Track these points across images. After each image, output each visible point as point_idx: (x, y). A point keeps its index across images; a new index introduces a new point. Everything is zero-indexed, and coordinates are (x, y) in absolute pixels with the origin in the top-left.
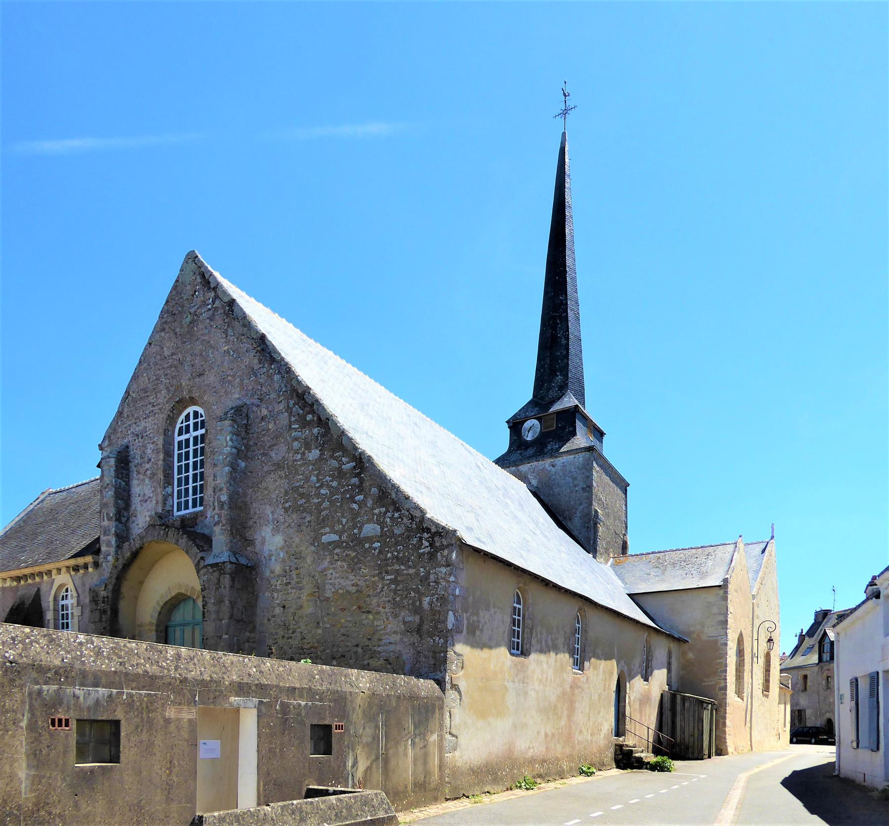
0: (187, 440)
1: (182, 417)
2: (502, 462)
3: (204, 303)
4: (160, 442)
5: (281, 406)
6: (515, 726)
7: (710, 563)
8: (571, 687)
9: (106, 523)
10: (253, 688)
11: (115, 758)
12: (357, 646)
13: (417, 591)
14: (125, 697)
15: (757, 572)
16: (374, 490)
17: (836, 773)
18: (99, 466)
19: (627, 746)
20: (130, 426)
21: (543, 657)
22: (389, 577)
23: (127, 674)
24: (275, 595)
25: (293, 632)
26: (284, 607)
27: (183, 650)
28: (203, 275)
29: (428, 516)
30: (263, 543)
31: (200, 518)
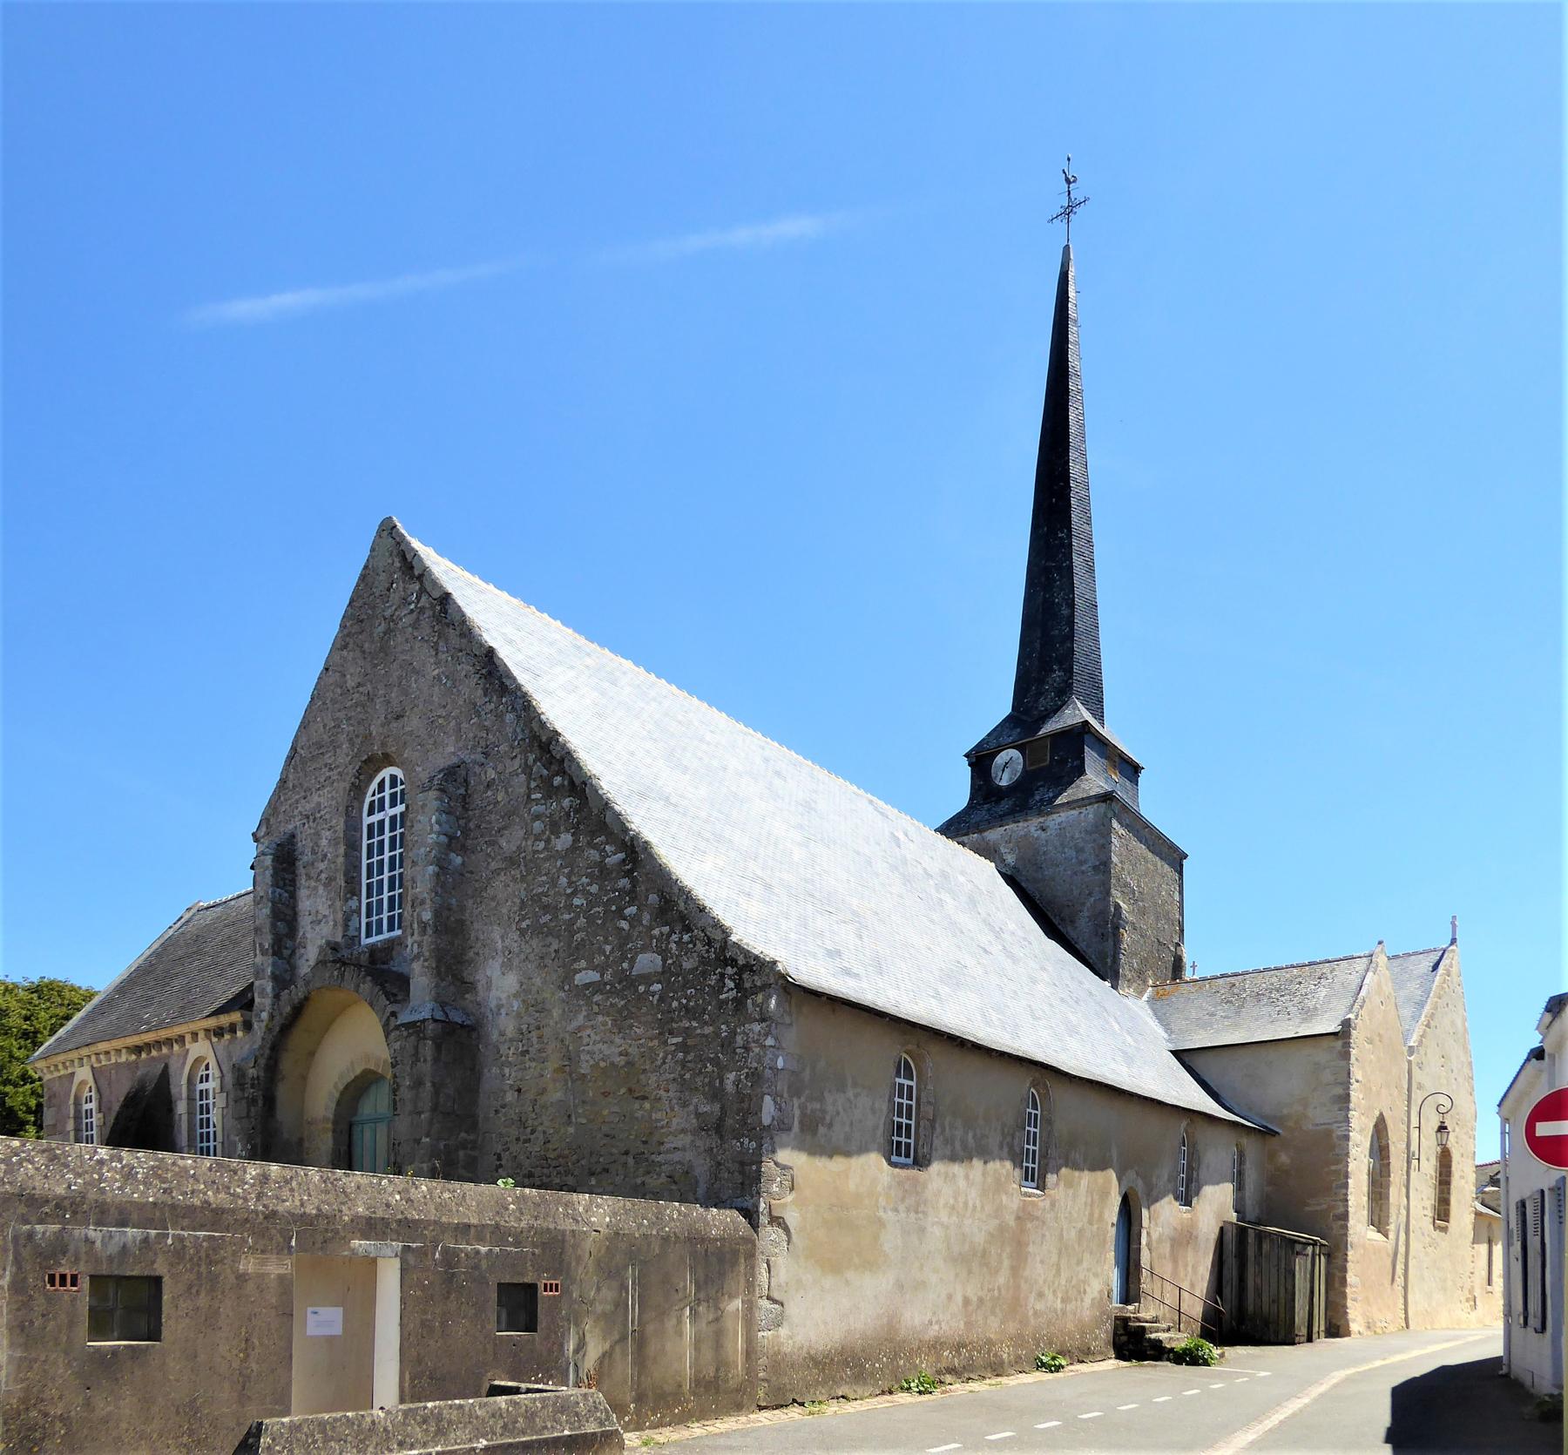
0: (381, 823)
1: (374, 785)
2: (953, 829)
3: (405, 601)
4: (341, 827)
5: (517, 763)
6: (900, 1286)
7: (1323, 992)
8: (1018, 1218)
9: (259, 959)
10: (394, 1225)
11: (154, 1335)
12: (627, 1153)
13: (716, 1062)
14: (170, 1241)
15: (1421, 1005)
16: (653, 898)
17: (1504, 1370)
18: (252, 867)
19: (1138, 1320)
20: (297, 802)
21: (957, 1169)
22: (675, 1040)
23: (173, 1207)
24: (507, 1071)
25: (533, 1132)
26: (519, 1090)
27: (274, 1168)
28: (403, 556)
29: (734, 938)
30: (489, 988)
31: (397, 948)
